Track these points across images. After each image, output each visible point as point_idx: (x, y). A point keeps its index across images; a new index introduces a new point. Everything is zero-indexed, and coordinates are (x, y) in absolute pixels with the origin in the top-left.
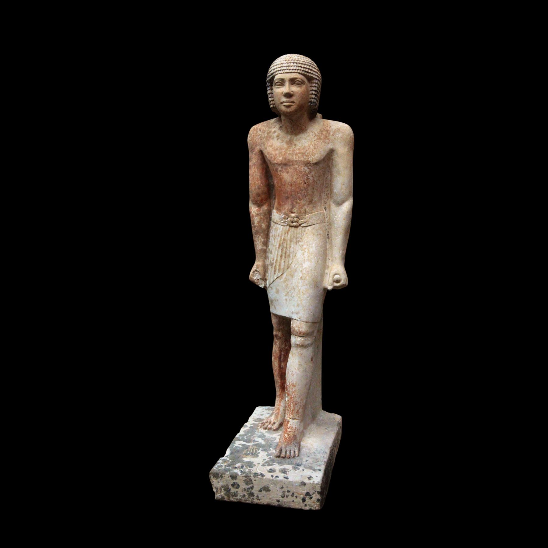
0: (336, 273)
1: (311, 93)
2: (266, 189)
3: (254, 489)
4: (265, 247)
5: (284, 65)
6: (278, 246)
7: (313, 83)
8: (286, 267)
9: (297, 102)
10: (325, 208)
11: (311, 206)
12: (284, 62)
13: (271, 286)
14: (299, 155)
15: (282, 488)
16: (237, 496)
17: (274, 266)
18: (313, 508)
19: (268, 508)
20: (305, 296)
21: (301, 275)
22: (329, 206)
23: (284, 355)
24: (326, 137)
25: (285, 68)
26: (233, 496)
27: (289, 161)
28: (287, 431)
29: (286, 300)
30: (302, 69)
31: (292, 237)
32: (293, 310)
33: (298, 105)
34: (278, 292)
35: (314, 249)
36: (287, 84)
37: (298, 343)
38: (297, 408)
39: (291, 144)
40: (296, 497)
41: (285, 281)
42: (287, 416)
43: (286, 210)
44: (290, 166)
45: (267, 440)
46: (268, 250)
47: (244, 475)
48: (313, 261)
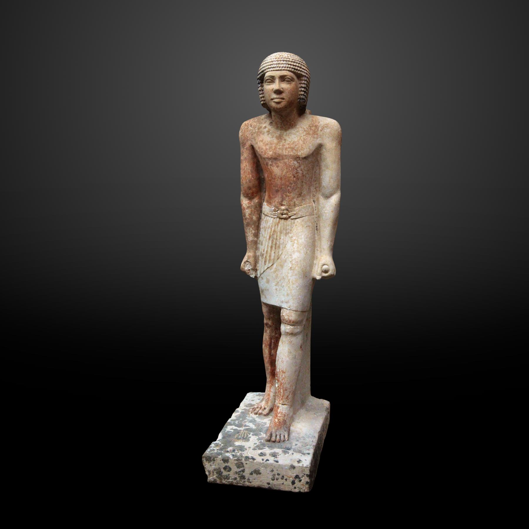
0: (324, 263)
1: (300, 89)
2: (257, 182)
3: (245, 472)
4: (256, 239)
5: (274, 63)
6: (268, 238)
7: (303, 80)
8: (276, 258)
9: (287, 99)
10: (314, 201)
11: (300, 198)
12: (274, 60)
13: (262, 276)
14: (289, 150)
15: (272, 471)
16: (229, 479)
17: (264, 256)
18: (302, 491)
19: (259, 491)
20: (295, 286)
21: (290, 265)
22: (318, 199)
23: (274, 343)
24: (315, 133)
25: (275, 66)
26: (225, 479)
27: (279, 155)
28: (277, 416)
29: (276, 289)
30: (292, 66)
31: (282, 229)
32: (283, 299)
33: (288, 102)
34: (268, 281)
35: (303, 240)
36: (277, 81)
37: (287, 331)
38: (286, 394)
39: (281, 139)
40: (286, 480)
41: (275, 272)
42: (277, 401)
43: (276, 203)
44: (280, 160)
45: (258, 425)
46: (258, 242)
47: (236, 458)
48: (302, 251)
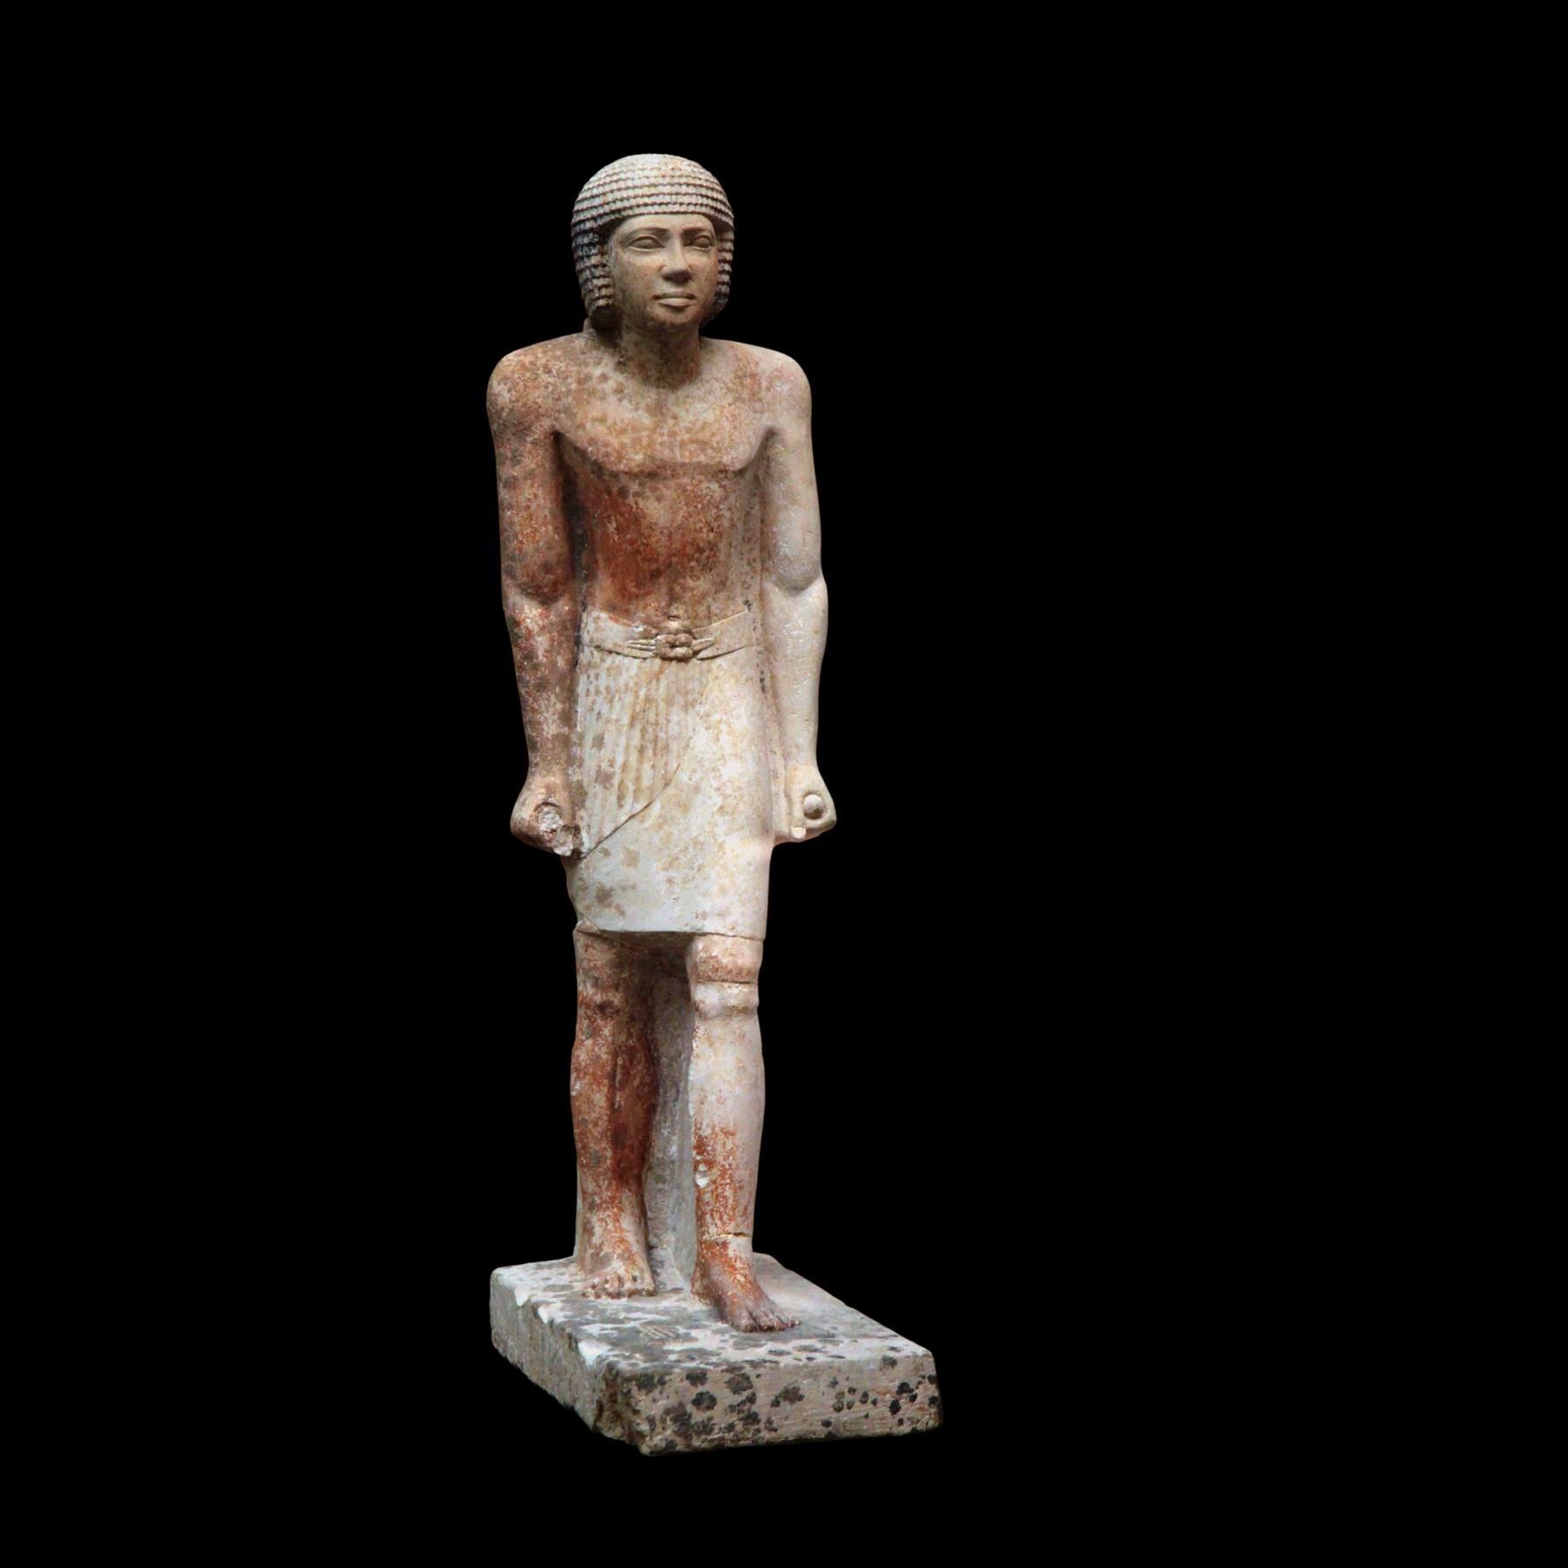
0: (804, 799)
5: (661, 189)
6: (625, 720)
8: (660, 784)
9: (701, 296)
10: (746, 602)
11: (722, 596)
12: (660, 180)
13: (604, 845)
14: (692, 447)
15: (834, 1383)
17: (616, 781)
18: (920, 1427)
19: (802, 1451)
21: (719, 801)
22: (762, 595)
23: (623, 1067)
24: (754, 396)
25: (667, 199)
26: (698, 1434)
27: (664, 465)
28: (733, 1267)
30: (711, 203)
31: (673, 688)
32: (706, 906)
33: (704, 307)
34: (632, 859)
35: (744, 721)
36: (677, 243)
37: (733, 1002)
38: (743, 1201)
40: (874, 1402)
41: (660, 826)
42: (713, 1230)
43: (651, 611)
44: (665, 478)
45: (666, 1312)
46: (574, 738)
48: (749, 756)
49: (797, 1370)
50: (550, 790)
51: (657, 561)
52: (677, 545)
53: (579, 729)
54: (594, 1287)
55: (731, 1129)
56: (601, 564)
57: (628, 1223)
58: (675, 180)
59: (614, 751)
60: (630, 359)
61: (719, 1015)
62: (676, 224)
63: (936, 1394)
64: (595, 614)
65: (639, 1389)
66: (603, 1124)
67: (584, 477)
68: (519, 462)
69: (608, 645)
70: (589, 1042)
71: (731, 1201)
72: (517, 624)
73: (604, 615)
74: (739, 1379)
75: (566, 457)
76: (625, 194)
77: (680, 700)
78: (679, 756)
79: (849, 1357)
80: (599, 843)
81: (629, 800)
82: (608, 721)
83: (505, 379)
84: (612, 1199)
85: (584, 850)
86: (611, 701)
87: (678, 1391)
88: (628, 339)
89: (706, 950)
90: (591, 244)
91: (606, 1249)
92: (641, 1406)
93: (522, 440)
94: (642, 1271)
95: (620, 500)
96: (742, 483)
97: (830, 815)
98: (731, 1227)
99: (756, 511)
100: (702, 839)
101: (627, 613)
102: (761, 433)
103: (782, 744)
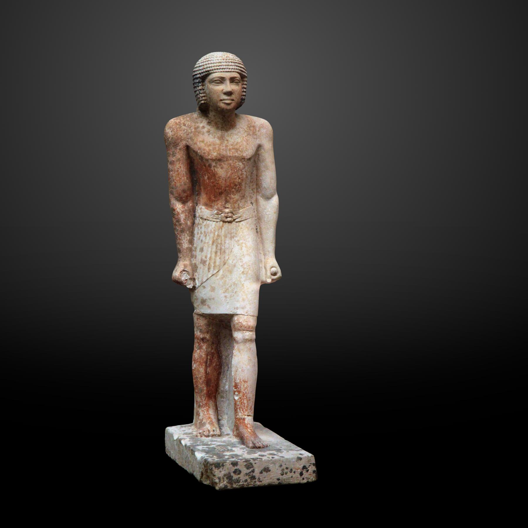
0: (270, 268)
5: (223, 64)
6: (211, 243)
8: (222, 264)
9: (236, 100)
10: (251, 203)
11: (243, 201)
12: (222, 61)
13: (204, 285)
14: (233, 151)
15: (281, 466)
17: (207, 263)
18: (310, 480)
19: (270, 489)
21: (242, 270)
22: (257, 200)
23: (210, 359)
24: (254, 133)
25: (225, 67)
26: (235, 483)
27: (224, 157)
28: (247, 427)
30: (239, 68)
31: (227, 232)
32: (238, 305)
34: (213, 289)
35: (251, 243)
36: (228, 82)
37: (247, 337)
38: (250, 405)
40: (294, 472)
41: (222, 278)
42: (240, 414)
43: (219, 206)
44: (224, 161)
45: (224, 442)
46: (193, 249)
48: (252, 255)
49: (268, 461)
50: (185, 266)
51: (221, 189)
52: (228, 184)
53: (195, 245)
54: (200, 433)
55: (246, 380)
56: (203, 190)
57: (211, 412)
58: (227, 61)
59: (207, 253)
60: (212, 121)
61: (242, 342)
62: (228, 75)
63: (315, 470)
64: (200, 207)
65: (215, 468)
66: (203, 379)
67: (197, 161)
68: (175, 156)
69: (205, 217)
70: (198, 351)
71: (246, 405)
72: (174, 210)
73: (203, 207)
74: (249, 464)
75: (191, 154)
76: (210, 65)
77: (229, 236)
78: (229, 255)
79: (286, 457)
80: (202, 284)
81: (212, 269)
82: (205, 243)
83: (170, 128)
84: (206, 404)
85: (197, 286)
86: (206, 236)
87: (228, 468)
88: (211, 114)
89: (238, 320)
90: (199, 82)
91: (204, 421)
92: (216, 474)
93: (176, 148)
94: (216, 428)
95: (209, 168)
96: (250, 163)
97: (279, 274)
98: (246, 413)
99: (255, 172)
100: (236, 282)
101: (211, 207)
102: (256, 146)
103: (263, 250)
